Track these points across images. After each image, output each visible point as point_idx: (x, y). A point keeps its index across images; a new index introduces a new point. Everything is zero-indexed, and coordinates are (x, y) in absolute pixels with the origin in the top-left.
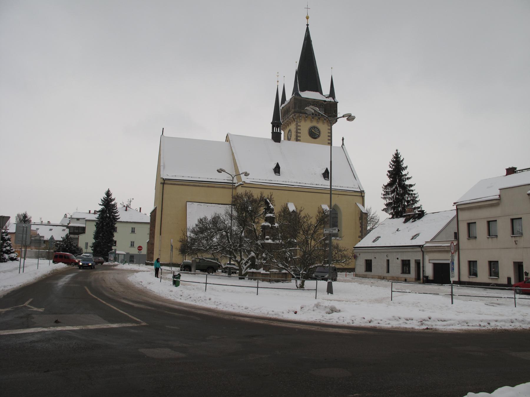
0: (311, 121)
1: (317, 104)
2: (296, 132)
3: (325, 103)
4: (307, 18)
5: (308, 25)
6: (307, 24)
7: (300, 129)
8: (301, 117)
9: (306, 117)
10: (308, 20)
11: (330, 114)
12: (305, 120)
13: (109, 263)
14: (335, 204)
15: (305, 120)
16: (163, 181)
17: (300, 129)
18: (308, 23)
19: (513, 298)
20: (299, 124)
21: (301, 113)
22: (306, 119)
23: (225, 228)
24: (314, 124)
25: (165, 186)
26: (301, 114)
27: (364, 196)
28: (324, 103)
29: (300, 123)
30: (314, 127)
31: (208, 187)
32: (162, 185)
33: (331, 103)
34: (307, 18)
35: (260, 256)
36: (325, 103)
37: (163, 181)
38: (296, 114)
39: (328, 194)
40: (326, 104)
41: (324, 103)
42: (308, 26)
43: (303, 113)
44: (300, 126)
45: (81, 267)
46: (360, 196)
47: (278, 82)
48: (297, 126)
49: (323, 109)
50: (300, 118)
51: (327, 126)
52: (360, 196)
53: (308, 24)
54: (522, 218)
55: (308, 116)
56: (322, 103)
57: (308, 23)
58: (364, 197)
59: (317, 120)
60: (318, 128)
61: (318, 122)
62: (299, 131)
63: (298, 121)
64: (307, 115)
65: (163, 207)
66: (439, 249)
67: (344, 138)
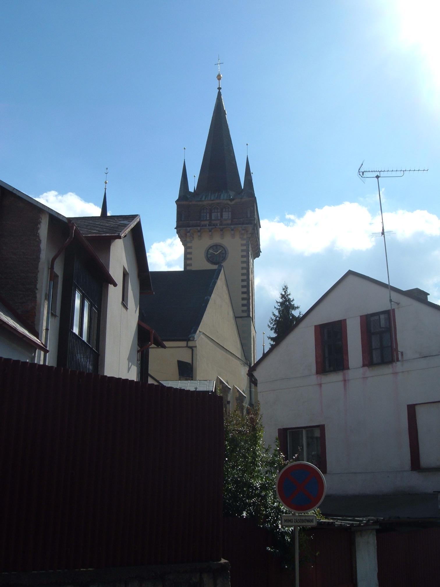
24: (217, 239)
27: (196, 347)
53: (218, 81)
58: (194, 348)
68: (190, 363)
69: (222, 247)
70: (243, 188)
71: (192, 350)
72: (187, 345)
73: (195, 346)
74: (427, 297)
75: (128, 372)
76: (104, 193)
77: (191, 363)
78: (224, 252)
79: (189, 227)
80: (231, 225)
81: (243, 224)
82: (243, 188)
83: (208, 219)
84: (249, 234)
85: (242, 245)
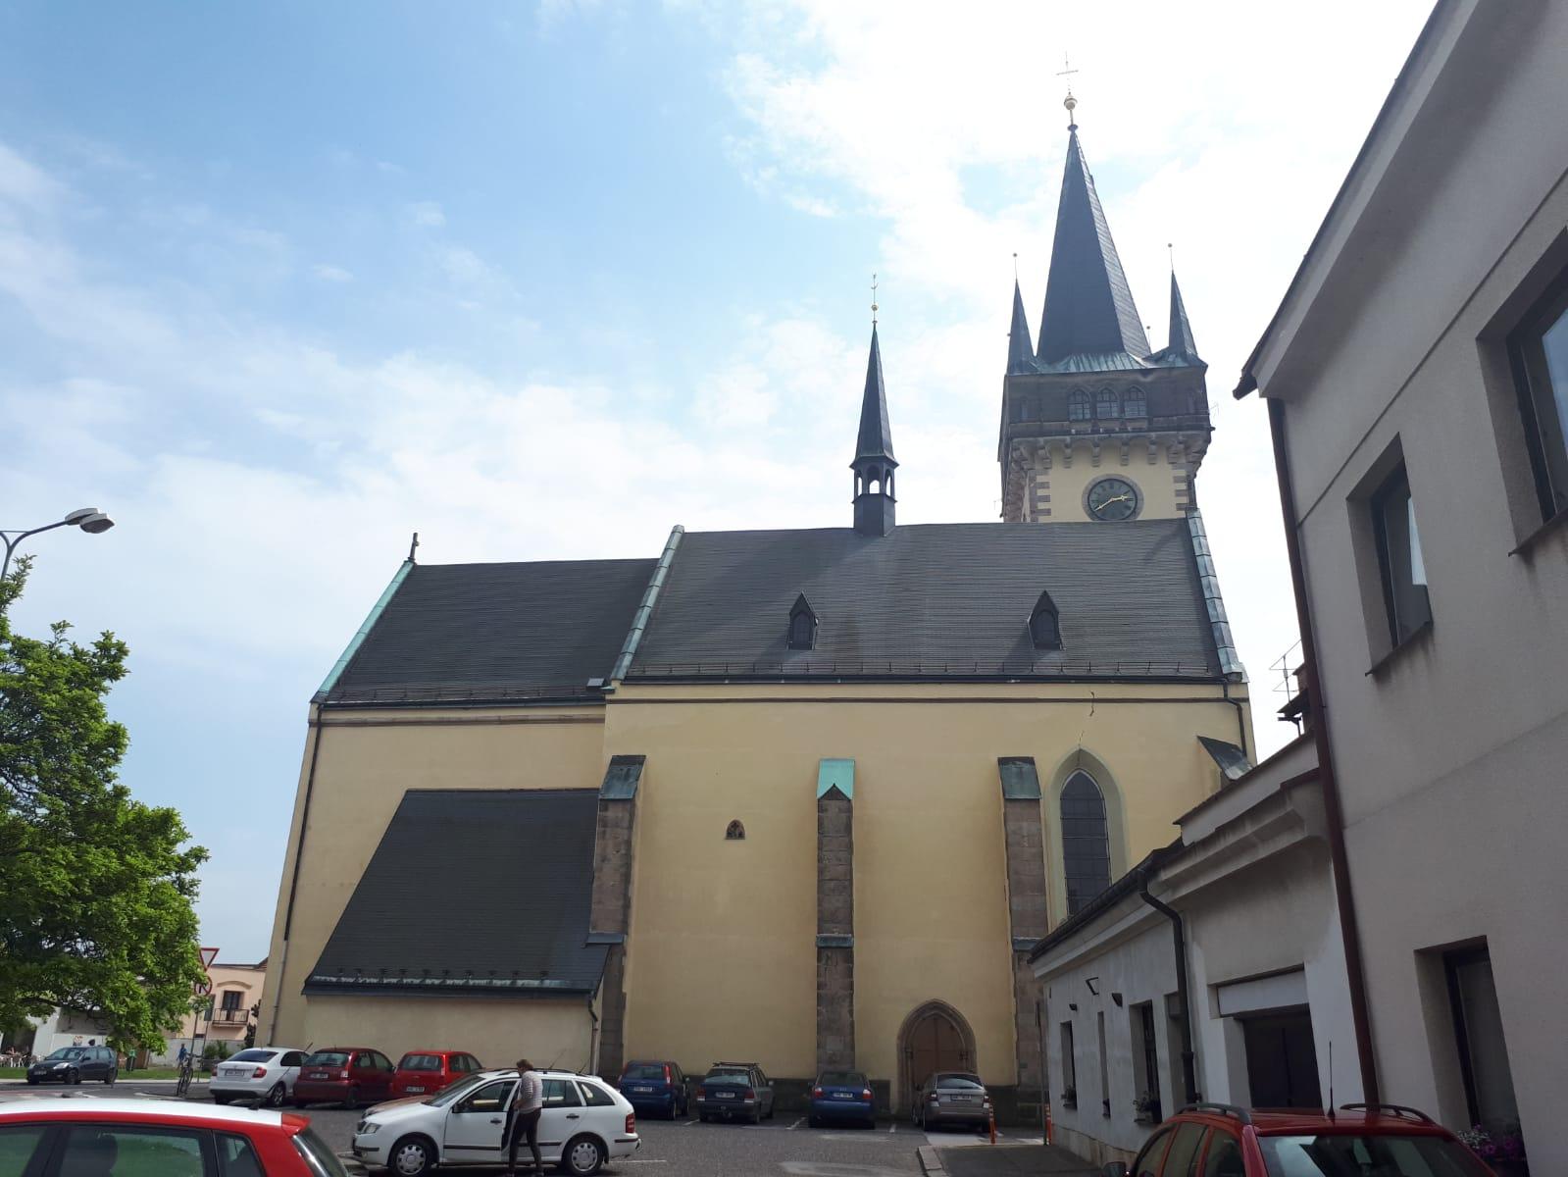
0: (1096, 463)
4: (1070, 104)
5: (1073, 128)
6: (1069, 124)
7: (1047, 499)
10: (1073, 111)
11: (1175, 418)
14: (1081, 750)
17: (1047, 499)
18: (1072, 121)
23: (112, 847)
24: (1110, 468)
25: (328, 734)
27: (1247, 700)
28: (1142, 379)
29: (1046, 474)
30: (1111, 481)
31: (501, 722)
33: (1175, 373)
34: (1070, 104)
36: (1149, 379)
40: (1151, 383)
41: (1142, 379)
42: (1077, 132)
46: (1217, 700)
47: (875, 308)
51: (1170, 466)
52: (1217, 700)
53: (1075, 123)
55: (1072, 442)
56: (1137, 382)
57: (1072, 121)
58: (1243, 705)
60: (1128, 482)
62: (1041, 506)
65: (311, 821)
66: (1244, 847)
68: (1235, 747)
69: (1124, 483)
70: (1035, 354)
71: (1240, 710)
72: (1226, 695)
73: (1245, 696)
74: (1320, 760)
75: (568, 1117)
76: (1006, 326)
77: (1240, 746)
78: (1132, 504)
79: (1042, 435)
80: (1150, 430)
81: (1179, 428)
82: (1035, 354)
83: (1088, 416)
84: (61, 678)
85: (1177, 480)
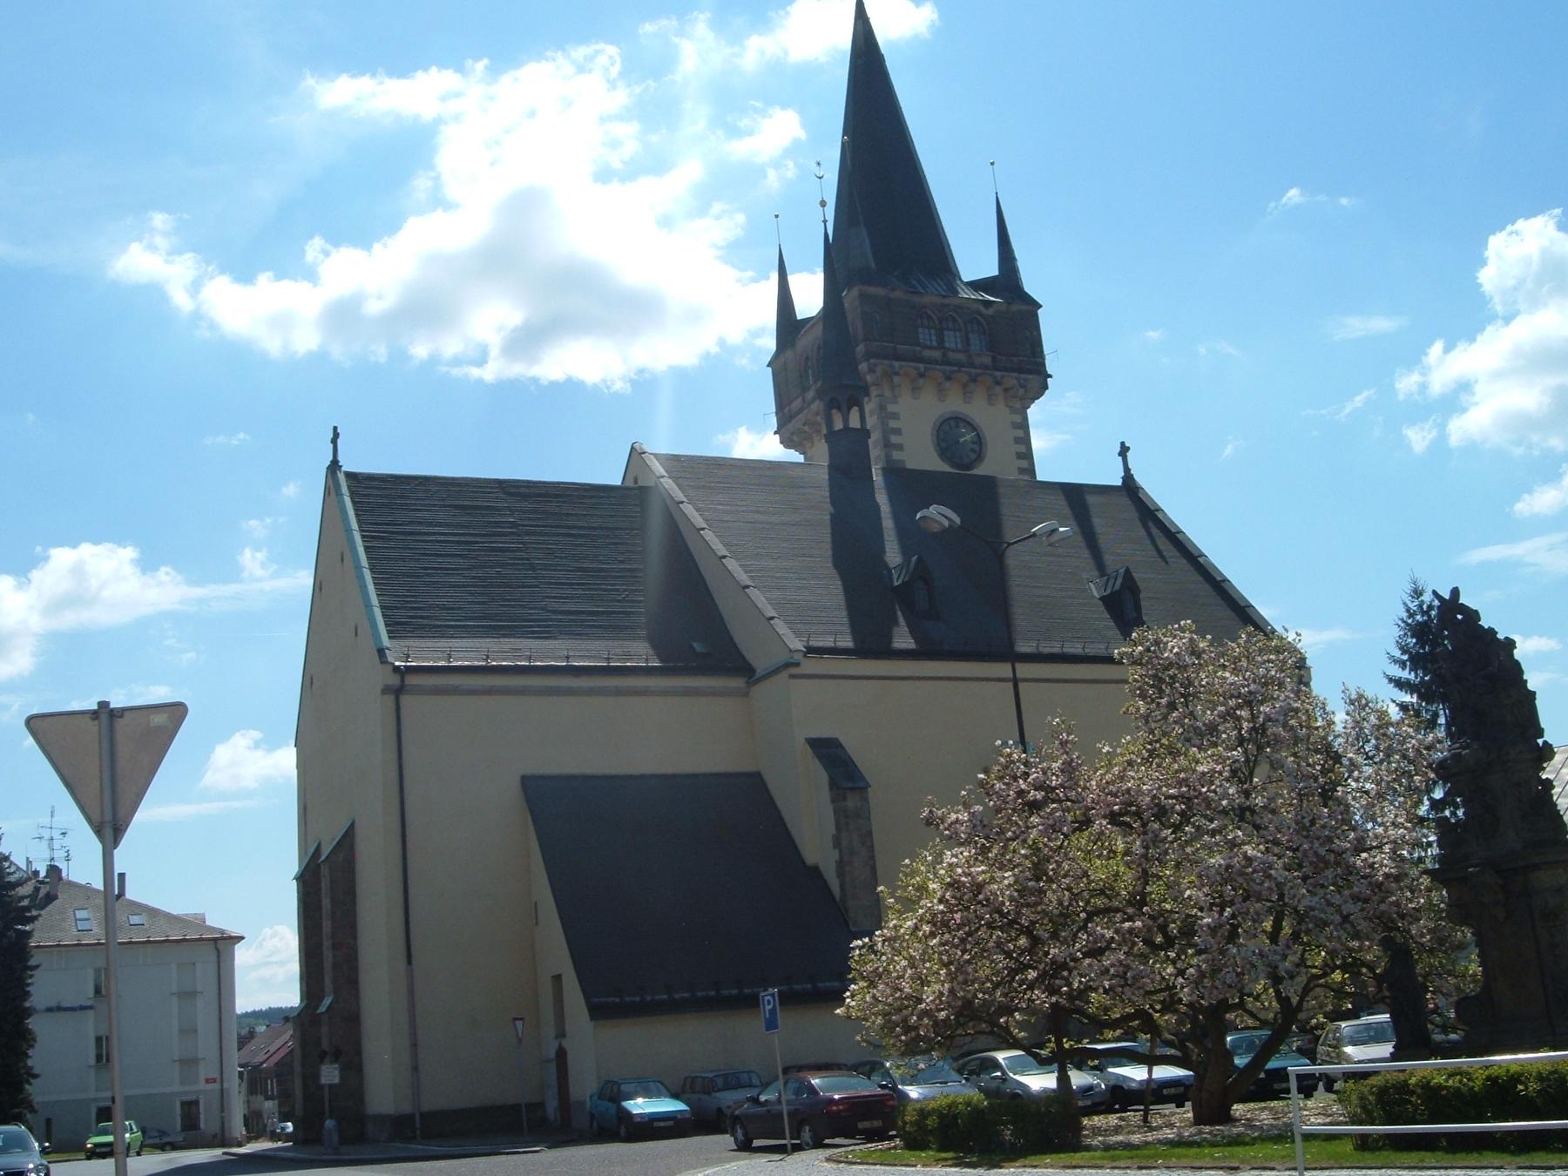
0: (941, 393)
1: (958, 318)
2: (885, 446)
3: (990, 311)
8: (897, 374)
9: (922, 375)
11: (1015, 359)
12: (916, 390)
13: (1193, 1051)
15: (916, 390)
16: (394, 680)
19: (80, 920)
20: (891, 408)
21: (898, 358)
22: (921, 381)
24: (955, 404)
25: (406, 700)
26: (897, 364)
28: (982, 309)
29: (896, 402)
30: (958, 420)
32: (390, 699)
35: (30, 912)
37: (394, 680)
38: (875, 365)
39: (1021, 691)
40: (992, 316)
41: (982, 309)
43: (904, 360)
44: (895, 416)
45: (343, 1070)
48: (885, 415)
49: (958, 334)
50: (896, 379)
54: (379, 689)
55: (926, 369)
59: (964, 386)
61: (967, 396)
63: (888, 393)
64: (922, 366)
67: (339, 431)
